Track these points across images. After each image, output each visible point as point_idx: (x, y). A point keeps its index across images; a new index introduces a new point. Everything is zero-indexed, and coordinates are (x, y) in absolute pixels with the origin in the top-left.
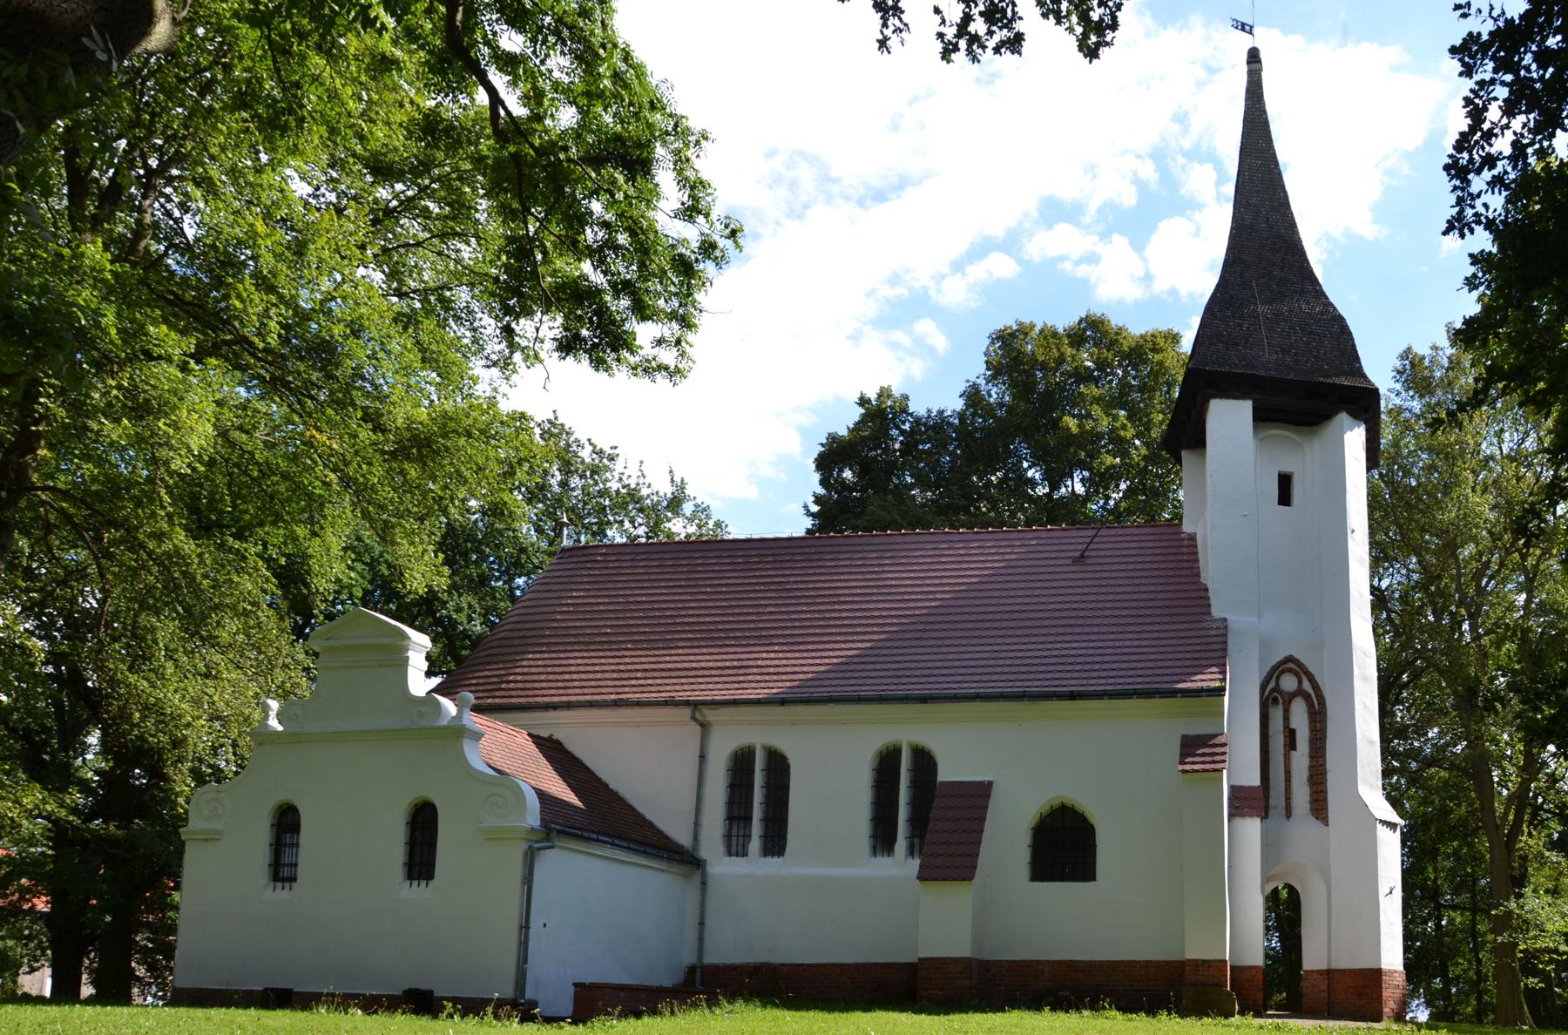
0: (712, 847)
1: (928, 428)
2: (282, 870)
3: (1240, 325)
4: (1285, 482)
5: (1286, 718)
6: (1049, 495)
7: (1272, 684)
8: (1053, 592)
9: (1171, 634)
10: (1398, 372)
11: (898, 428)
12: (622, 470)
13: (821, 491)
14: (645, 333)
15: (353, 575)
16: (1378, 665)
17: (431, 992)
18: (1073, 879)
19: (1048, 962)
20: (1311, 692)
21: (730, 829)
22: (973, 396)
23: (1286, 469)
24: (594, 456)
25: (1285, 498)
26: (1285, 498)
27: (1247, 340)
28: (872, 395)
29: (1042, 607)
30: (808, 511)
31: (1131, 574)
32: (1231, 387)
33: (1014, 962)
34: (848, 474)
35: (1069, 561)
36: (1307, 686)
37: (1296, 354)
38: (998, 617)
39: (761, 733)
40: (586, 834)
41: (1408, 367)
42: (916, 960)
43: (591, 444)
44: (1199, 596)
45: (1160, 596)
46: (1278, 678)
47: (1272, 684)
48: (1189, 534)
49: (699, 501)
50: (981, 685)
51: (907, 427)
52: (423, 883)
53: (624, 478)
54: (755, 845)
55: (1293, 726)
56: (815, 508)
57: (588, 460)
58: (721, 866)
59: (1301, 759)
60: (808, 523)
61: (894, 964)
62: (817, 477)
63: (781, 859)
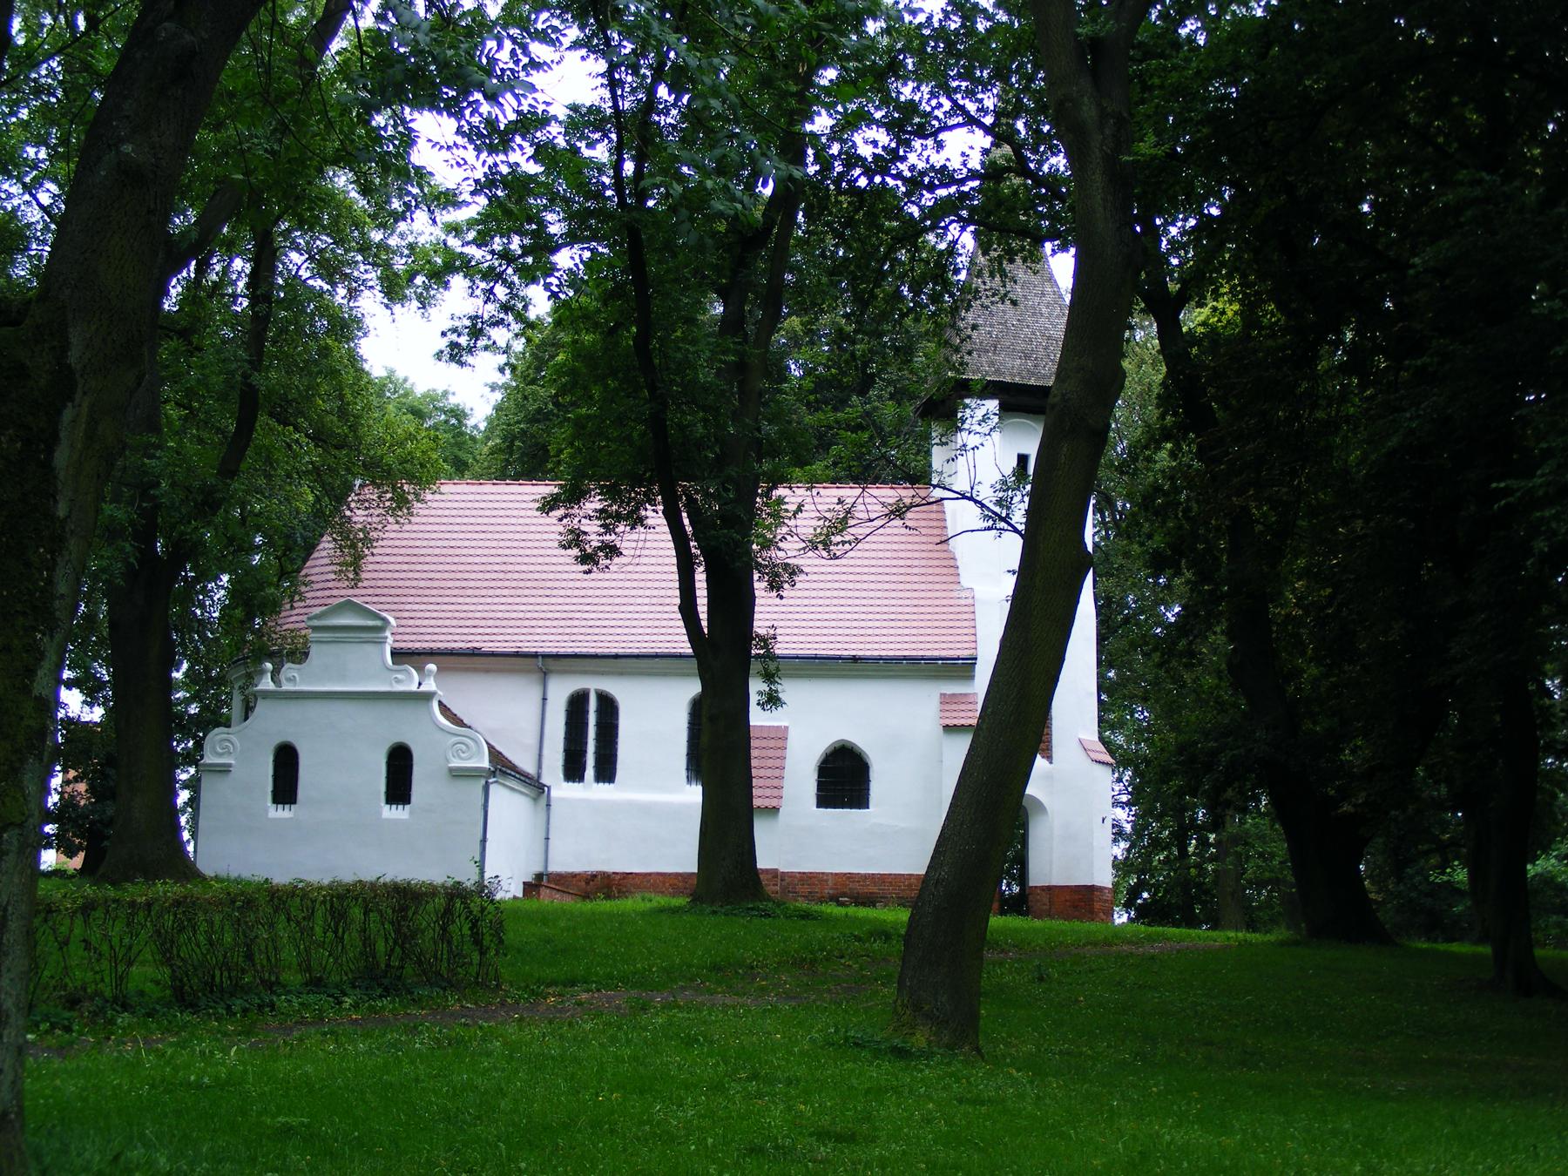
15: (198, 951)
16: (1101, 677)
18: (851, 807)
37: (1036, 359)
39: (594, 684)
45: (916, 563)
52: (400, 807)
54: (590, 772)
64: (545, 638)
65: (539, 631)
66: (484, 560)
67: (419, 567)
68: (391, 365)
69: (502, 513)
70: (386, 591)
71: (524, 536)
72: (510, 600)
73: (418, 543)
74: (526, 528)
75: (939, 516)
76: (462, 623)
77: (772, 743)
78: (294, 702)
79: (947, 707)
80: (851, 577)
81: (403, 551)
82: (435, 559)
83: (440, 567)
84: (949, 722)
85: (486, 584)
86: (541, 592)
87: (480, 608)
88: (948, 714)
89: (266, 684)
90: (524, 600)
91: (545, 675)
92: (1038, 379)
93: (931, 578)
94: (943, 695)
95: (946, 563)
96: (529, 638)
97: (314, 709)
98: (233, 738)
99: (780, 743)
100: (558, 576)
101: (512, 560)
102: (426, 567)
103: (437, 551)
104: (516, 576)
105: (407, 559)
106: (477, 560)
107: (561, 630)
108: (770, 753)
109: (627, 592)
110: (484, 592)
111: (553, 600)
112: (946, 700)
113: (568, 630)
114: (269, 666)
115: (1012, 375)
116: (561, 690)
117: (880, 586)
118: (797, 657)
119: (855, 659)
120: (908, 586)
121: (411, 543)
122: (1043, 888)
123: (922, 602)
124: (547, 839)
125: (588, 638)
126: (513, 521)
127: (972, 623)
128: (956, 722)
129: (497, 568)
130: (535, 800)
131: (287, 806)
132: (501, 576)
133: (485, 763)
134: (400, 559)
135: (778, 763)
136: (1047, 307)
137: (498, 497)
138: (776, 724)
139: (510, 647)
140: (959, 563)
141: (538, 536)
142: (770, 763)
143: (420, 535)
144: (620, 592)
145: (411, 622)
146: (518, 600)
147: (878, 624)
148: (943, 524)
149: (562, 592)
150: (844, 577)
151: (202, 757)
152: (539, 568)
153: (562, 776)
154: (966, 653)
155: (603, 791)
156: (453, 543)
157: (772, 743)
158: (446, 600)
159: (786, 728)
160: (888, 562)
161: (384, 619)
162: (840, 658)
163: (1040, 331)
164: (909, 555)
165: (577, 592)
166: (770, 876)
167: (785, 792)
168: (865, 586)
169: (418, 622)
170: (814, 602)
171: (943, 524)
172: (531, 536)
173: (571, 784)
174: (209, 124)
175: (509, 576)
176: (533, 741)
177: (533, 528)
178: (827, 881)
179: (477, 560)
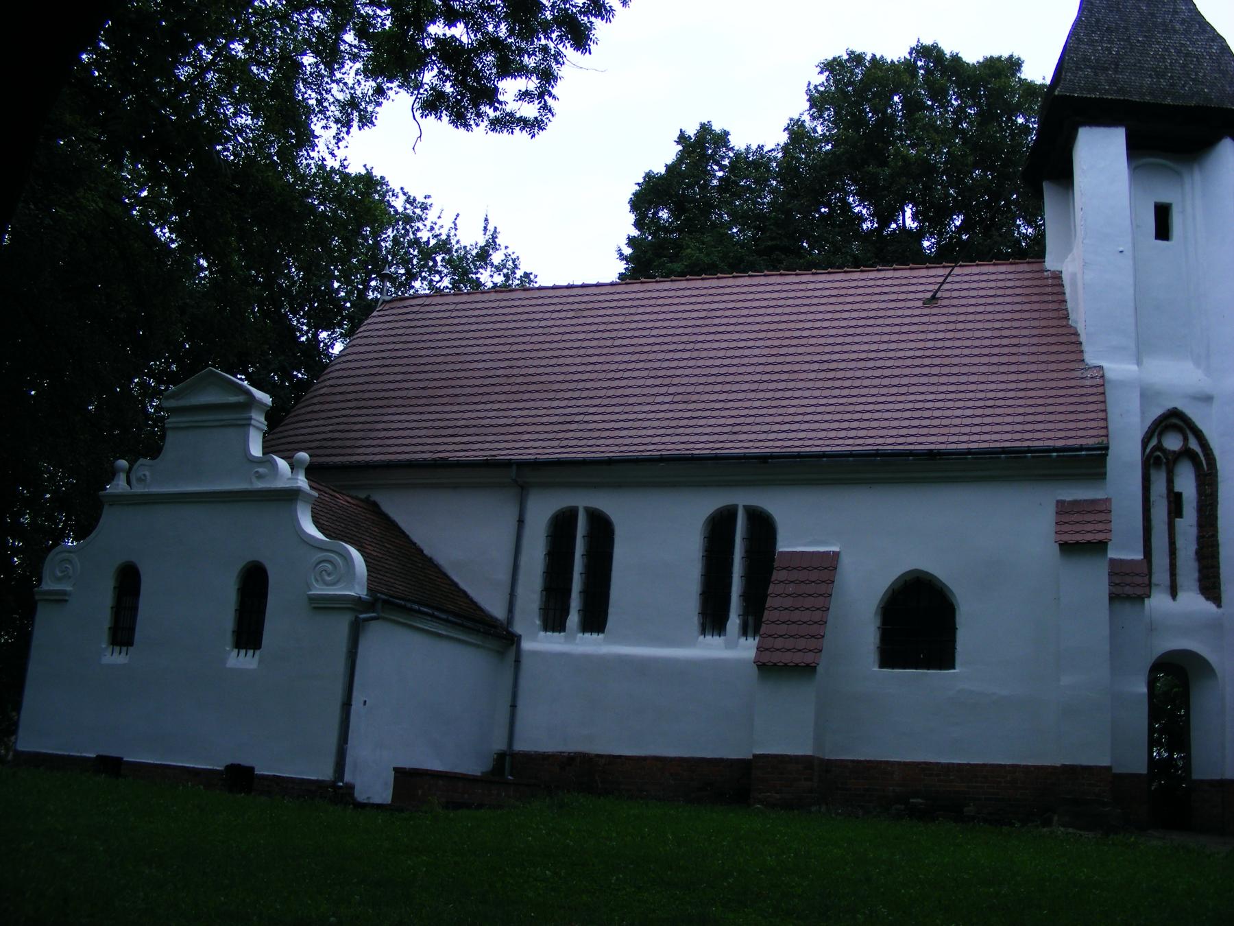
1: (749, 164)
2: (122, 634)
3: (1109, 50)
5: (1170, 482)
6: (879, 230)
7: (1154, 442)
8: (904, 337)
11: (717, 163)
12: (435, 219)
13: (635, 232)
14: (509, 88)
17: (252, 769)
19: (899, 763)
21: (837, 564)
22: (797, 132)
23: (1164, 199)
24: (408, 206)
25: (1163, 230)
26: (1163, 230)
27: (1117, 65)
28: (691, 131)
30: (621, 254)
31: (990, 317)
33: (859, 762)
34: (664, 214)
35: (920, 304)
36: (1194, 445)
37: (1171, 77)
38: (842, 365)
39: (582, 500)
40: (409, 605)
42: (750, 757)
43: (405, 194)
44: (1072, 342)
47: (1154, 442)
48: (1054, 272)
49: (509, 251)
50: (828, 442)
51: (726, 162)
52: (251, 652)
53: (436, 227)
54: (574, 619)
55: (1177, 489)
56: (628, 251)
57: (400, 210)
59: (1188, 524)
60: (621, 267)
61: (721, 760)
62: (632, 218)
63: (601, 636)
75: (1056, 290)
77: (814, 576)
84: (1066, 538)
89: (119, 485)
93: (1044, 358)
94: (1060, 503)
95: (1065, 339)
100: (569, 377)
108: (811, 588)
111: (555, 403)
112: (1064, 510)
119: (931, 455)
124: (514, 706)
128: (1078, 537)
130: (501, 654)
138: (822, 549)
140: (1083, 338)
142: (809, 602)
148: (1060, 297)
151: (40, 581)
154: (1091, 442)
157: (814, 576)
159: (836, 555)
161: (248, 393)
163: (1175, 48)
168: (955, 370)
171: (1060, 297)
174: (337, 20)
176: (504, 576)
177: (553, 330)
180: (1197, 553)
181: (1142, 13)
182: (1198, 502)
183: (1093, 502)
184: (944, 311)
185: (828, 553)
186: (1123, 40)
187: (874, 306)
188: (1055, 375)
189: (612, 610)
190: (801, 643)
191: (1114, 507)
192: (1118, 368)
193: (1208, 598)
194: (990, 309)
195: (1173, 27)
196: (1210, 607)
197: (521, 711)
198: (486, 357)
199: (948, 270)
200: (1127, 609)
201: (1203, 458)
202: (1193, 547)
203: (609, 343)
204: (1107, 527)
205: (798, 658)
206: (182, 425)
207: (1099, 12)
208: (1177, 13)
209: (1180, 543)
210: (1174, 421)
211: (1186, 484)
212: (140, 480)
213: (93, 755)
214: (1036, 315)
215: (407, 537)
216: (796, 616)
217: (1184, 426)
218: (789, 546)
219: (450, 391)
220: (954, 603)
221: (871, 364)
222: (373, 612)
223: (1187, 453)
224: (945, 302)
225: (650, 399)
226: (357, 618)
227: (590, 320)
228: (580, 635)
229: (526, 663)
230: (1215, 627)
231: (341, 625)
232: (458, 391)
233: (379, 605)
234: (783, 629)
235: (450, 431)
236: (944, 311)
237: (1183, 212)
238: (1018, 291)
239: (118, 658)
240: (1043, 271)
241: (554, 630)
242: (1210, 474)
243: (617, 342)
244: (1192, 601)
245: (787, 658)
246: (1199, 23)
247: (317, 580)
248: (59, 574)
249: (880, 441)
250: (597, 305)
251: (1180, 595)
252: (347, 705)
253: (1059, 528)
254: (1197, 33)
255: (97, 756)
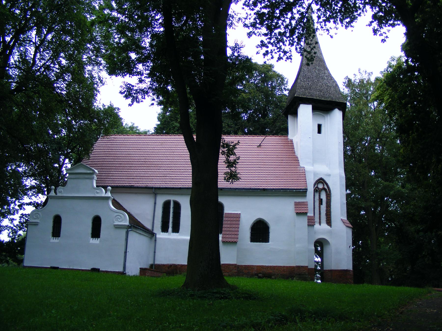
0: (157, 229)
4: (319, 126)
5: (320, 196)
7: (316, 186)
9: (289, 171)
10: (344, 83)
20: (327, 188)
25: (319, 132)
26: (319, 132)
27: (310, 88)
29: (250, 161)
32: (306, 101)
33: (246, 265)
36: (326, 187)
37: (324, 92)
39: (172, 198)
41: (347, 81)
44: (296, 160)
45: (284, 159)
46: (318, 184)
47: (316, 186)
48: (291, 140)
52: (96, 239)
54: (170, 229)
58: (161, 235)
59: (324, 207)
63: (178, 234)
64: (156, 182)
65: (154, 180)
66: (139, 158)
67: (117, 160)
68: (133, 122)
69: (146, 144)
70: (105, 168)
71: (153, 151)
72: (146, 170)
73: (118, 153)
74: (153, 148)
75: (292, 145)
76: (129, 177)
77: (235, 219)
78: (61, 200)
79: (297, 206)
80: (262, 164)
81: (112, 155)
82: (123, 158)
83: (124, 160)
84: (298, 211)
85: (138, 165)
86: (157, 168)
87: (136, 173)
88: (298, 209)
90: (151, 170)
91: (155, 195)
92: (325, 98)
95: (294, 159)
96: (151, 182)
97: (68, 203)
98: (39, 213)
99: (237, 219)
100: (163, 163)
101: (148, 158)
102: (119, 160)
103: (123, 155)
104: (149, 163)
105: (113, 158)
106: (136, 158)
107: (162, 180)
108: (234, 222)
109: (185, 168)
110: (137, 168)
111: (160, 171)
112: (296, 204)
113: (164, 180)
114: (53, 187)
115: (316, 97)
116: (161, 200)
117: (272, 166)
118: (244, 189)
119: (264, 190)
120: (282, 166)
121: (115, 153)
122: (329, 271)
123: (287, 171)
124: (155, 252)
125: (171, 182)
126: (150, 146)
127: (305, 178)
128: (300, 211)
129: (143, 160)
130: (151, 238)
131: (57, 238)
132: (144, 163)
133: (127, 223)
134: (111, 158)
135: (237, 226)
136: (326, 77)
137: (145, 139)
138: (236, 212)
139: (144, 185)
140: (299, 159)
141: (157, 151)
142: (234, 226)
143: (119, 151)
144: (183, 168)
145: (112, 177)
146: (149, 170)
147: (272, 178)
148: (293, 147)
149: (164, 168)
150: (260, 164)
152: (157, 160)
153: (160, 230)
154: (303, 188)
155: (175, 236)
156: (129, 153)
157: (235, 219)
158: (125, 170)
159: (240, 214)
160: (275, 159)
161: (93, 170)
162: (259, 189)
164: (282, 156)
165: (168, 168)
166: (233, 267)
167: (239, 236)
169: (114, 177)
170: (249, 171)
171: (293, 147)
172: (155, 151)
173: (164, 233)
175: (146, 163)
176: (151, 218)
178: (254, 268)
179: (136, 158)
180: (326, 214)
181: (316, 73)
182: (326, 201)
183: (303, 202)
184: (263, 149)
185: (238, 213)
186: (312, 81)
187: (244, 147)
188: (293, 169)
189: (181, 227)
190: (233, 236)
191: (309, 204)
192: (308, 168)
193: (328, 225)
194: (275, 149)
195: (324, 78)
196: (329, 227)
197: (156, 253)
198: (137, 155)
199: (264, 138)
200: (310, 227)
201: (328, 190)
202: (325, 212)
203: (172, 153)
204: (307, 209)
205: (232, 240)
206: (73, 178)
207: (306, 72)
208: (325, 73)
209: (322, 211)
210: (321, 181)
211: (323, 196)
212: (60, 192)
213: (50, 267)
214: (287, 152)
215: (122, 206)
216: (231, 229)
217: (323, 182)
218: (227, 211)
219: (129, 165)
220: (269, 226)
221: (245, 163)
222: (131, 229)
223: (324, 189)
224: (263, 147)
225: (187, 171)
226: (127, 230)
227: (166, 146)
228: (172, 233)
229: (158, 241)
230: (330, 232)
231: (124, 232)
232: (131, 165)
233: (132, 227)
234: (228, 233)
235: (132, 177)
236: (263, 149)
237: (325, 126)
238: (282, 145)
239: (55, 240)
240: (288, 139)
241: (165, 232)
242: (329, 194)
243: (175, 153)
244: (324, 226)
245: (230, 240)
246: (330, 77)
247: (116, 221)
248: (35, 217)
249: (250, 185)
250: (167, 142)
251: (322, 224)
252: (126, 252)
253: (296, 209)
254: (330, 80)
255: (51, 267)
